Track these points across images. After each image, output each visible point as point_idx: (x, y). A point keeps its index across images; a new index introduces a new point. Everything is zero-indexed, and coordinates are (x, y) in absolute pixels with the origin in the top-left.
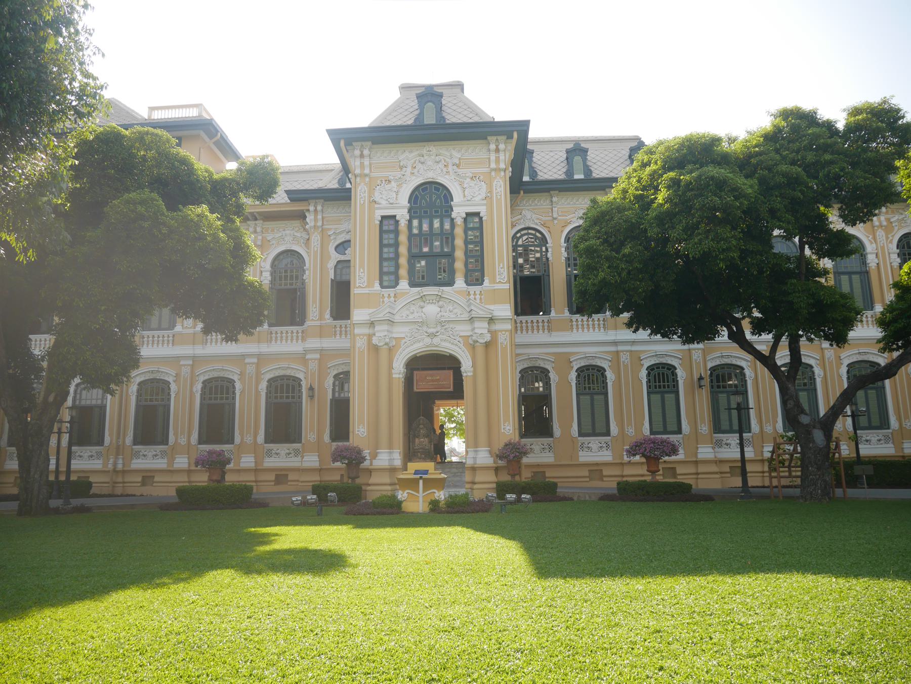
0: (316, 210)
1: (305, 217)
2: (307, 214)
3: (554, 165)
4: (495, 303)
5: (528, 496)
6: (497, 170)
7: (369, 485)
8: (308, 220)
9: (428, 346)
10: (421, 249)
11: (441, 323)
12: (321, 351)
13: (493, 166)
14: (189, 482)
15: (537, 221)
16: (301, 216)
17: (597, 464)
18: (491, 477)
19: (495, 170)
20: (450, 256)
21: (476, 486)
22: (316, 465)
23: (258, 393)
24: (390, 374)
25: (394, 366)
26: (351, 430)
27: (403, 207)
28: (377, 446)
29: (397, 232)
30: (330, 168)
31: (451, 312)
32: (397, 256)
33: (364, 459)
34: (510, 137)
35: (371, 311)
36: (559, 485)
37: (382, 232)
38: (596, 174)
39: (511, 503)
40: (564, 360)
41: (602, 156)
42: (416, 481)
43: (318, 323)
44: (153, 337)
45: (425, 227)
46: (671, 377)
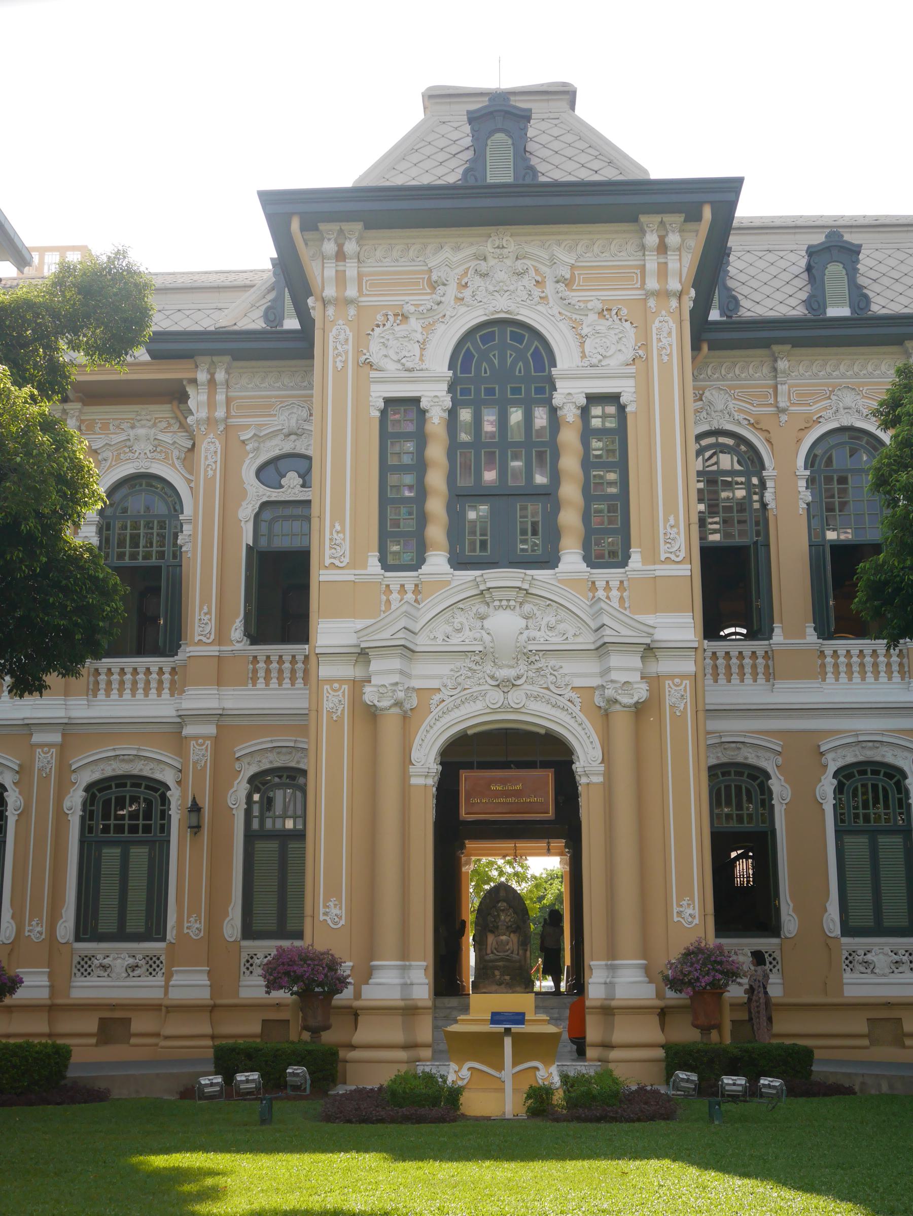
0: (212, 382)
1: (183, 397)
2: (190, 390)
3: (777, 283)
4: (656, 609)
5: (777, 1083)
6: (663, 294)
7: (353, 1047)
8: (191, 403)
9: (495, 711)
10: (479, 476)
11: (528, 656)
12: (219, 717)
13: (652, 284)
14: (213, 1037)
15: (741, 417)
16: (177, 395)
17: (888, 1005)
18: (650, 1032)
19: (656, 294)
20: (549, 496)
21: (614, 1054)
22: (203, 995)
23: (61, 816)
24: (405, 776)
25: (415, 755)
26: (308, 910)
27: (437, 379)
28: (371, 952)
29: (421, 438)
30: (241, 280)
31: (551, 628)
32: (422, 492)
33: (342, 983)
34: (694, 216)
35: (360, 624)
36: (817, 1054)
37: (386, 436)
38: (880, 306)
39: (734, 1098)
40: (810, 748)
41: (892, 262)
42: (495, 1040)
43: (213, 650)
44: (135, 671)
45: (489, 426)
46: (893, 796)
